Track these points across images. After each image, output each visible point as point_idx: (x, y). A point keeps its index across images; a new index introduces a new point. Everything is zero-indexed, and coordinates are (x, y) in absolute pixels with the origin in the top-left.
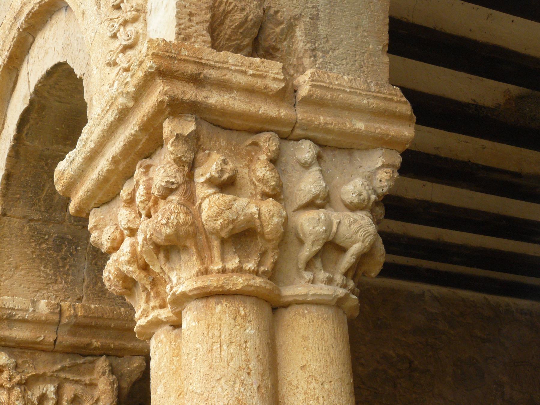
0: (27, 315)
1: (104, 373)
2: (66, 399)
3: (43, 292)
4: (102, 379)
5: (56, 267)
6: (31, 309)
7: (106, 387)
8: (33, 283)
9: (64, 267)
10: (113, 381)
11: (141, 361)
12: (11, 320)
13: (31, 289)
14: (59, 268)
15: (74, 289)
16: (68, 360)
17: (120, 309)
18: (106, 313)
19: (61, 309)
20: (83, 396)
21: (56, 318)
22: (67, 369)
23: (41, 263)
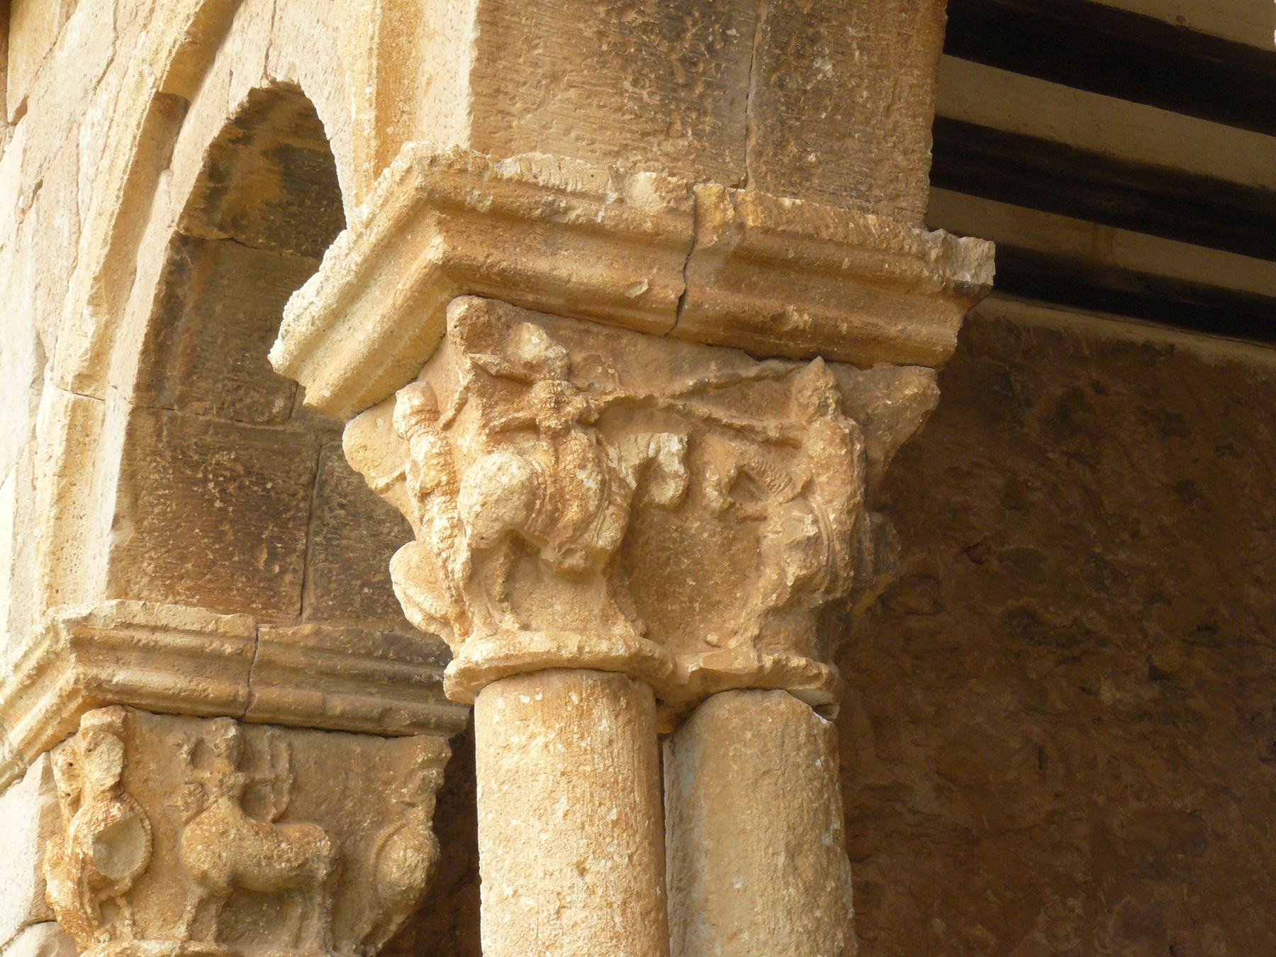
0: (601, 214)
1: (822, 409)
2: (715, 478)
3: (632, 159)
4: (817, 425)
5: (668, 87)
6: (613, 196)
7: (831, 450)
8: (602, 128)
9: (688, 86)
10: (851, 433)
11: (924, 381)
12: (556, 224)
13: (597, 146)
14: (675, 90)
15: (722, 155)
16: (713, 366)
17: (865, 219)
18: (827, 227)
19: (696, 201)
20: (762, 473)
21: (682, 227)
22: (712, 392)
23: (624, 69)
